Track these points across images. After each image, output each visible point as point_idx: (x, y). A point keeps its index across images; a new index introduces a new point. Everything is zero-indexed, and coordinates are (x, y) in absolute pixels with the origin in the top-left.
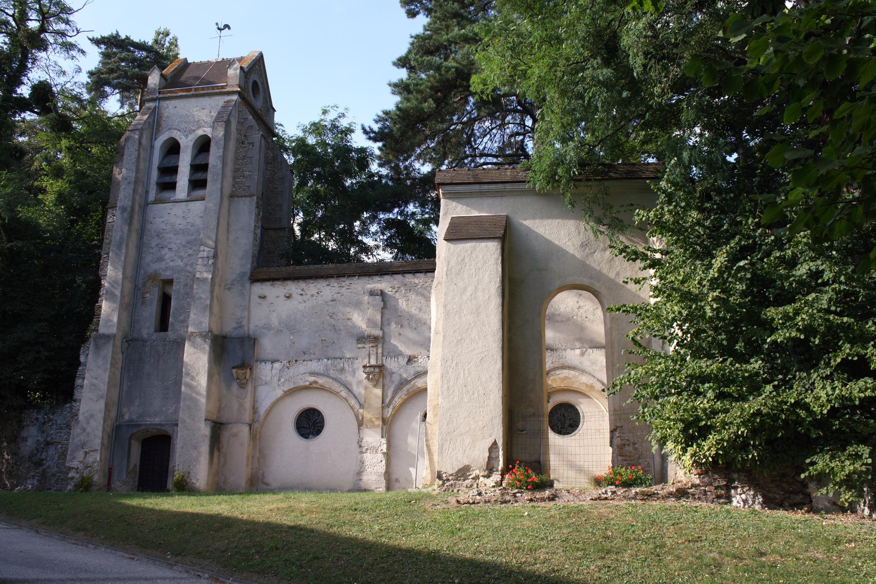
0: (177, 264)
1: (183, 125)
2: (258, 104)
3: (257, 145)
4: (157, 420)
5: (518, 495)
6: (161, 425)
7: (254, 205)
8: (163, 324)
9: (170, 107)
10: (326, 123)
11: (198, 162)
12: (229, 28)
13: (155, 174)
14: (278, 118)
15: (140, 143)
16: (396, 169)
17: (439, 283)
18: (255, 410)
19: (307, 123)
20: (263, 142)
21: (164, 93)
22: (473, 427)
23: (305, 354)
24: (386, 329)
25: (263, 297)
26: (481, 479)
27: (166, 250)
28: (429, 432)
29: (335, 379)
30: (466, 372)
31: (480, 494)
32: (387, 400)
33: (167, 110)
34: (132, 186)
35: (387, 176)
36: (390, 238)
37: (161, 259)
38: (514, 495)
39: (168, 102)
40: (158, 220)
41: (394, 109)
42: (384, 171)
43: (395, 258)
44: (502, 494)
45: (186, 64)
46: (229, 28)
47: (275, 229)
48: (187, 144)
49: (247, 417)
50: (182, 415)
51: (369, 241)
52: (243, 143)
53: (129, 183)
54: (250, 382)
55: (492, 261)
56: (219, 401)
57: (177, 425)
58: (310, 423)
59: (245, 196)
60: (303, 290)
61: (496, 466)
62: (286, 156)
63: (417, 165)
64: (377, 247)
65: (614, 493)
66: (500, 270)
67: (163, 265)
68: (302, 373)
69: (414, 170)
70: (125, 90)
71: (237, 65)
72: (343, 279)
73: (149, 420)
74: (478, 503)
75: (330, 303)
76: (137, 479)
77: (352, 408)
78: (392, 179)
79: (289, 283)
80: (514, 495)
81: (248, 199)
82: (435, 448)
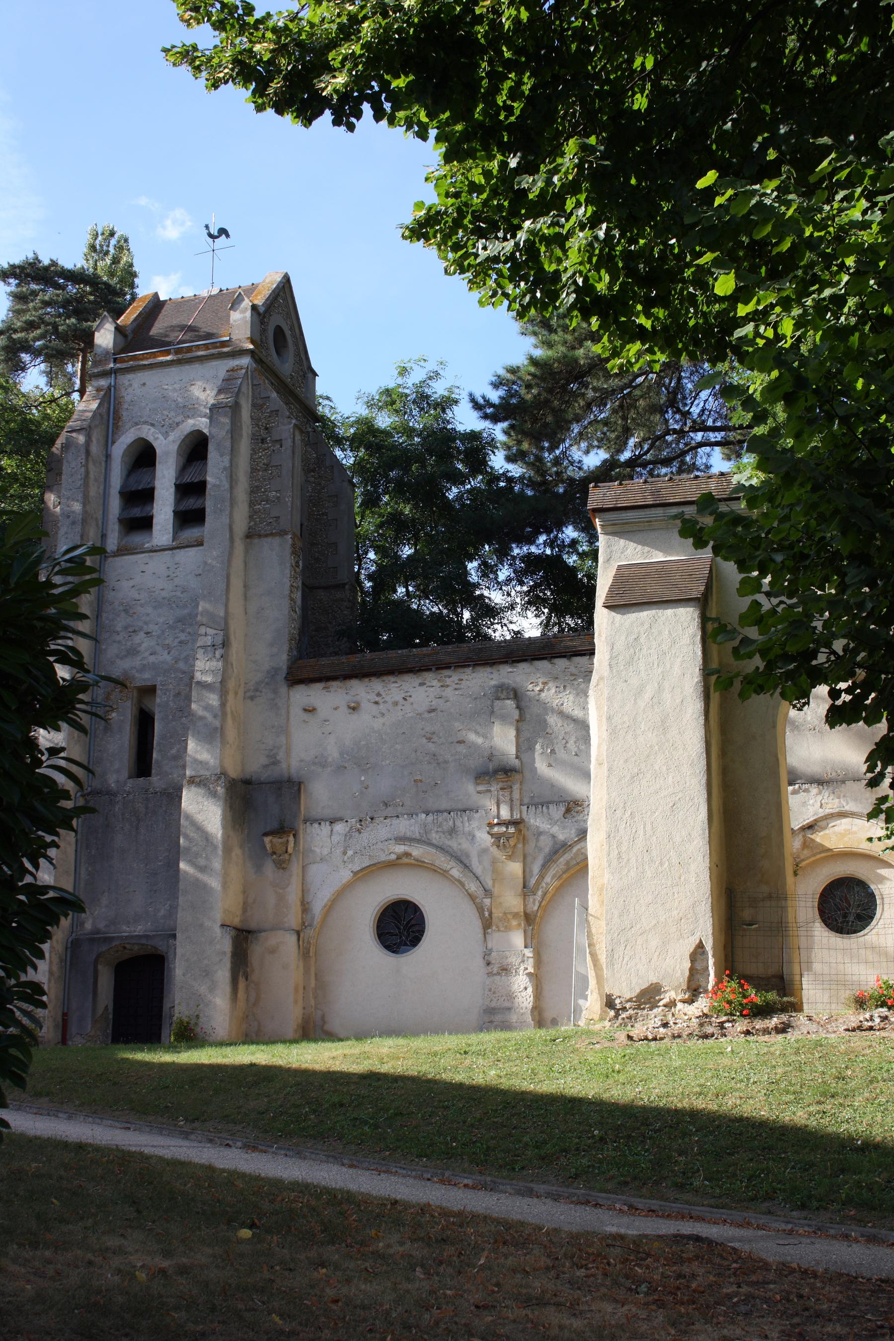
0: (161, 658)
1: (158, 417)
2: (286, 368)
3: (288, 443)
4: (139, 929)
5: (727, 1025)
6: (147, 937)
7: (288, 550)
8: (143, 765)
9: (136, 385)
10: (407, 391)
11: (187, 479)
12: (228, 236)
13: (115, 504)
14: (321, 387)
15: (88, 453)
16: (538, 464)
17: (601, 678)
18: (305, 907)
19: (373, 389)
20: (298, 437)
21: (122, 361)
22: (662, 919)
23: (388, 806)
24: (525, 757)
25: (310, 710)
26: (680, 1006)
27: (142, 634)
28: (594, 930)
29: (441, 848)
30: (649, 827)
31: (665, 1025)
32: (533, 881)
33: (130, 390)
34: (78, 528)
35: (522, 478)
36: (532, 589)
37: (133, 652)
38: (721, 1025)
39: (130, 376)
40: (125, 585)
41: (526, 362)
42: (516, 470)
43: (546, 625)
44: (701, 1025)
45: (156, 305)
46: (228, 236)
47: (326, 588)
48: (168, 449)
49: (293, 919)
50: (183, 917)
51: (496, 597)
52: (263, 441)
53: (74, 523)
54: (294, 858)
55: (686, 640)
56: (244, 892)
57: (174, 936)
58: (401, 927)
59: (272, 534)
60: (379, 695)
61: (703, 984)
62: (338, 453)
63: (576, 453)
64: (512, 607)
65: (884, 1018)
66: (700, 653)
67: (137, 662)
68: (382, 838)
69: (572, 463)
70: (55, 358)
71: (246, 303)
72: (446, 672)
73: (126, 930)
74: (662, 1039)
75: (426, 715)
76: (109, 1031)
77: (472, 897)
78: (532, 483)
79: (354, 683)
80: (721, 1025)
81: (276, 541)
82: (603, 958)
